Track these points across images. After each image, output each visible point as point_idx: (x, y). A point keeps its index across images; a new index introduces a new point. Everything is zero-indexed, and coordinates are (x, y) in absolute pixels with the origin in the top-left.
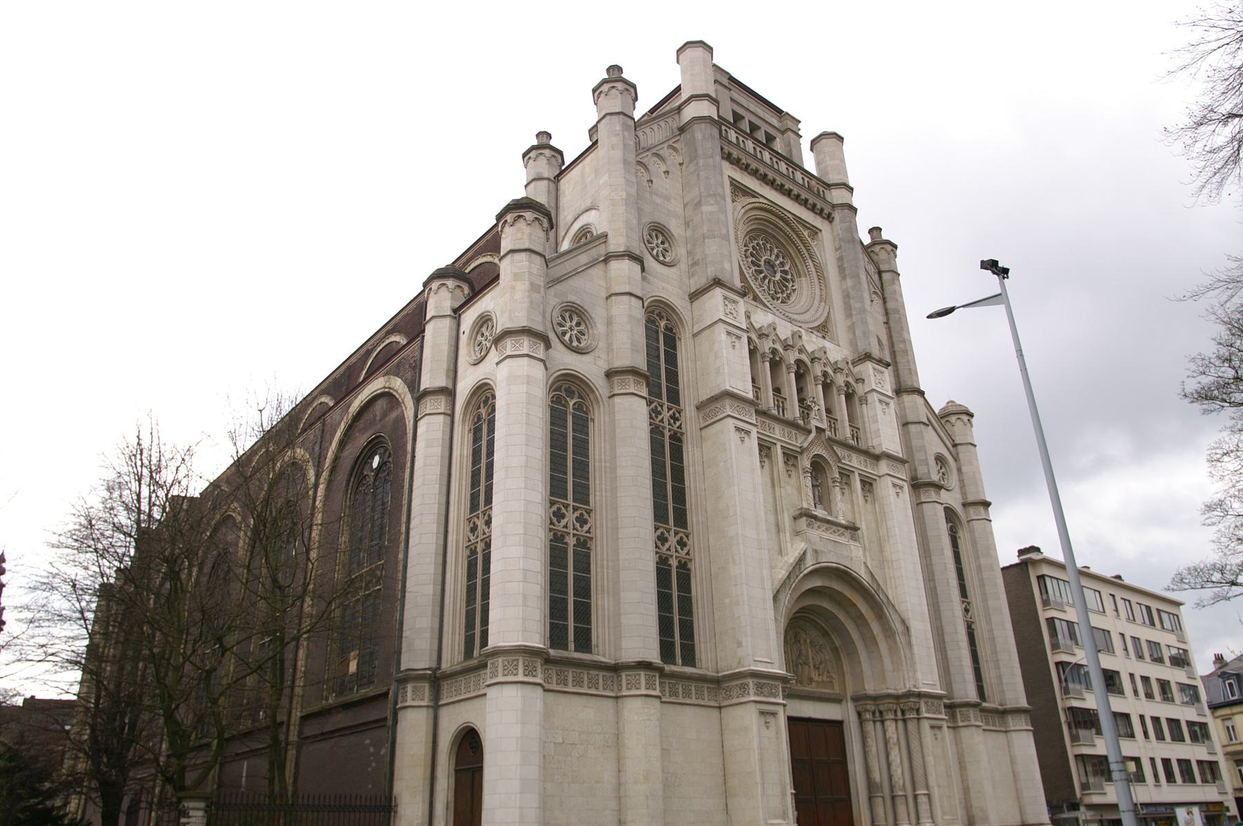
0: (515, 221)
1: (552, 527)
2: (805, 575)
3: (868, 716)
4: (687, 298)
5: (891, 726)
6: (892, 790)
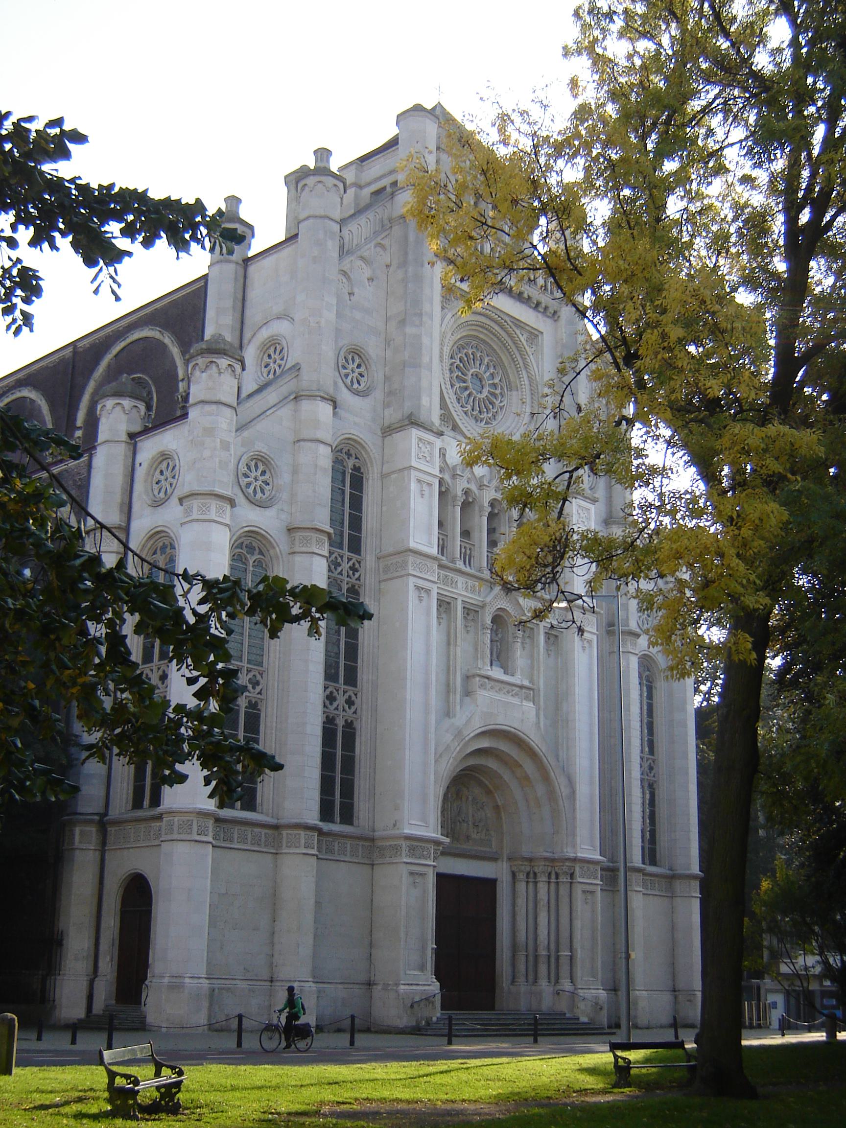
0: (207, 366)
3: (521, 876)
4: (380, 433)
5: (543, 888)
6: (536, 950)
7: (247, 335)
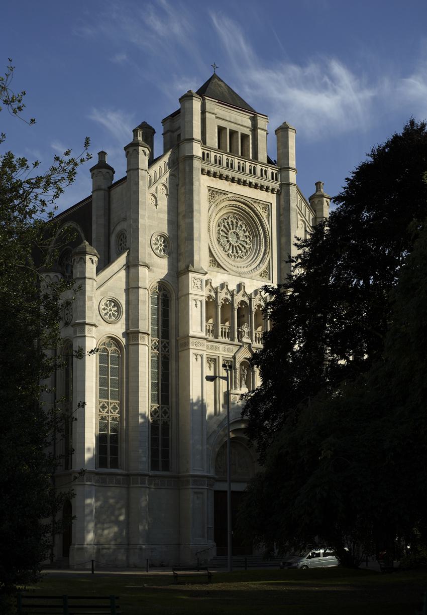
1: (100, 413)
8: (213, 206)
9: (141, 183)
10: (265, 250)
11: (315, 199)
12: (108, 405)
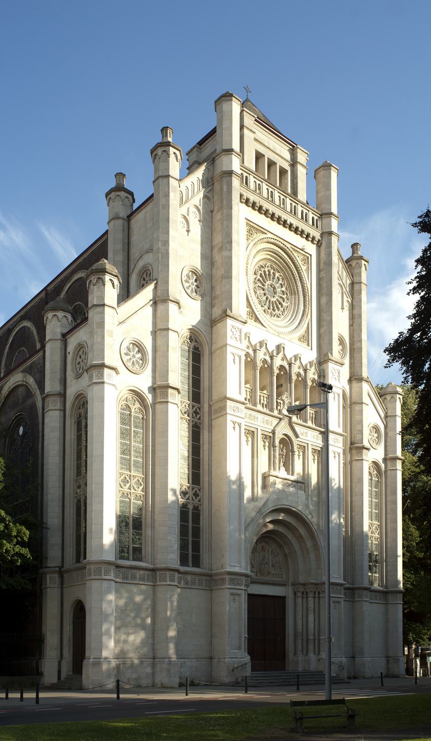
2: (267, 514)
3: (299, 594)
6: (307, 636)
7: (132, 267)
8: (252, 244)
9: (172, 195)
10: (304, 311)
11: (353, 261)
12: (130, 479)
